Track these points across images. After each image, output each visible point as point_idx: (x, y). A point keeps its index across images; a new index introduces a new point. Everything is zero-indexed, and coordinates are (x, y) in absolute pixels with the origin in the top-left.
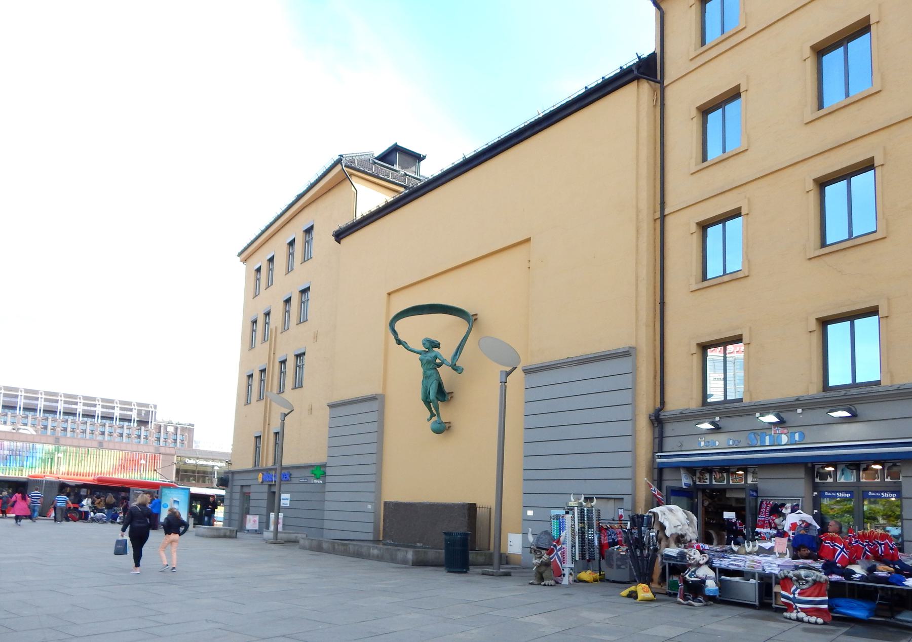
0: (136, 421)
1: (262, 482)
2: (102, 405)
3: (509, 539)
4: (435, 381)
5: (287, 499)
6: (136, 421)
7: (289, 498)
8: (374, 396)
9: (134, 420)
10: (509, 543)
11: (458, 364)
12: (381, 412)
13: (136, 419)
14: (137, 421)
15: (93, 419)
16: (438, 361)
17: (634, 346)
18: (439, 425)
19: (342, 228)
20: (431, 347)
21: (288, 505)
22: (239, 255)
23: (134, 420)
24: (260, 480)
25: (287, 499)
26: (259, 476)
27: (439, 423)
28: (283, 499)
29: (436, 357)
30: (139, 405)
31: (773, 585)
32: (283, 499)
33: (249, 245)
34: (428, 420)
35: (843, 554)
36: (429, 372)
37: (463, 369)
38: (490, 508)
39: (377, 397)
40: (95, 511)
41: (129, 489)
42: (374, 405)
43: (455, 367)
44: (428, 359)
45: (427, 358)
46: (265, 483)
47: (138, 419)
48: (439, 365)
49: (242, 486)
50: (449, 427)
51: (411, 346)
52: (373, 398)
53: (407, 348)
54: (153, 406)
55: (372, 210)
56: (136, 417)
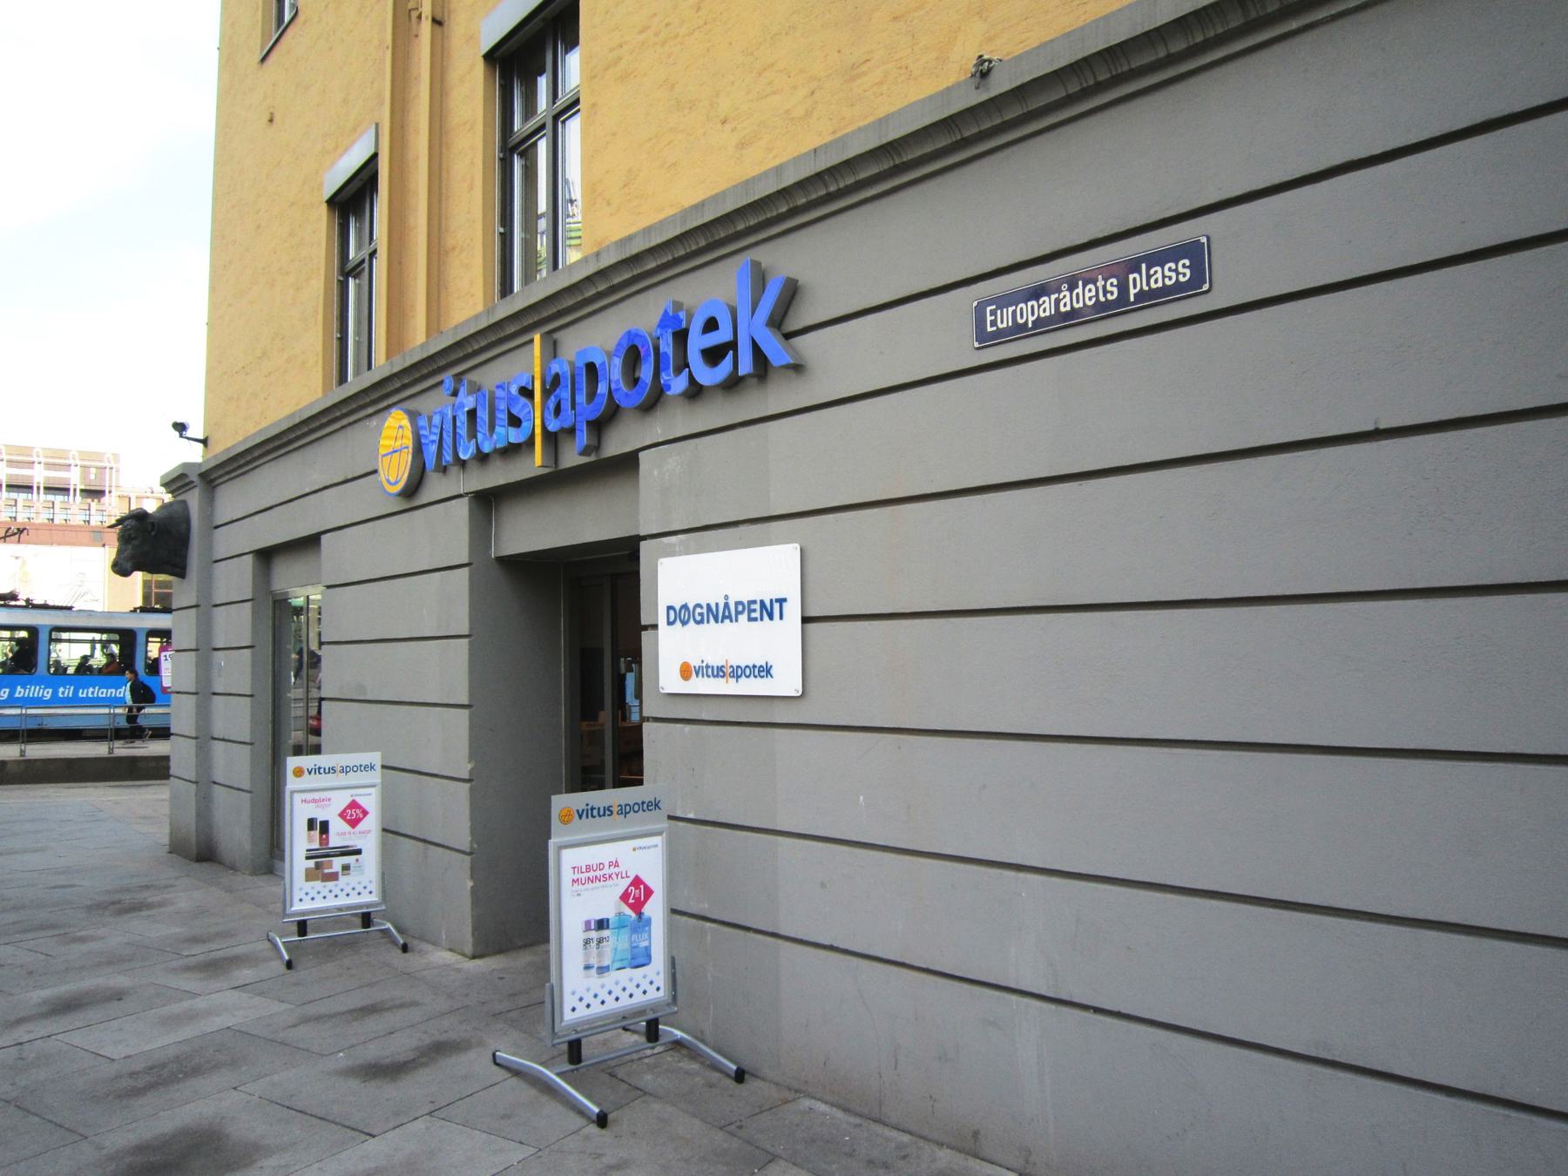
0: (78, 492)
1: (412, 489)
2: (46, 464)
5: (768, 610)
6: (78, 492)
7: (791, 590)
9: (75, 490)
13: (79, 487)
14: (82, 491)
15: (30, 495)
17: (583, 1057)
19: (652, 257)
21: (787, 682)
22: (308, 850)
23: (75, 490)
24: (396, 472)
25: (768, 610)
26: (386, 443)
28: (682, 615)
30: (84, 455)
31: (26, 758)
32: (682, 615)
46: (436, 487)
47: (83, 487)
49: (266, 556)
54: (111, 458)
56: (78, 483)
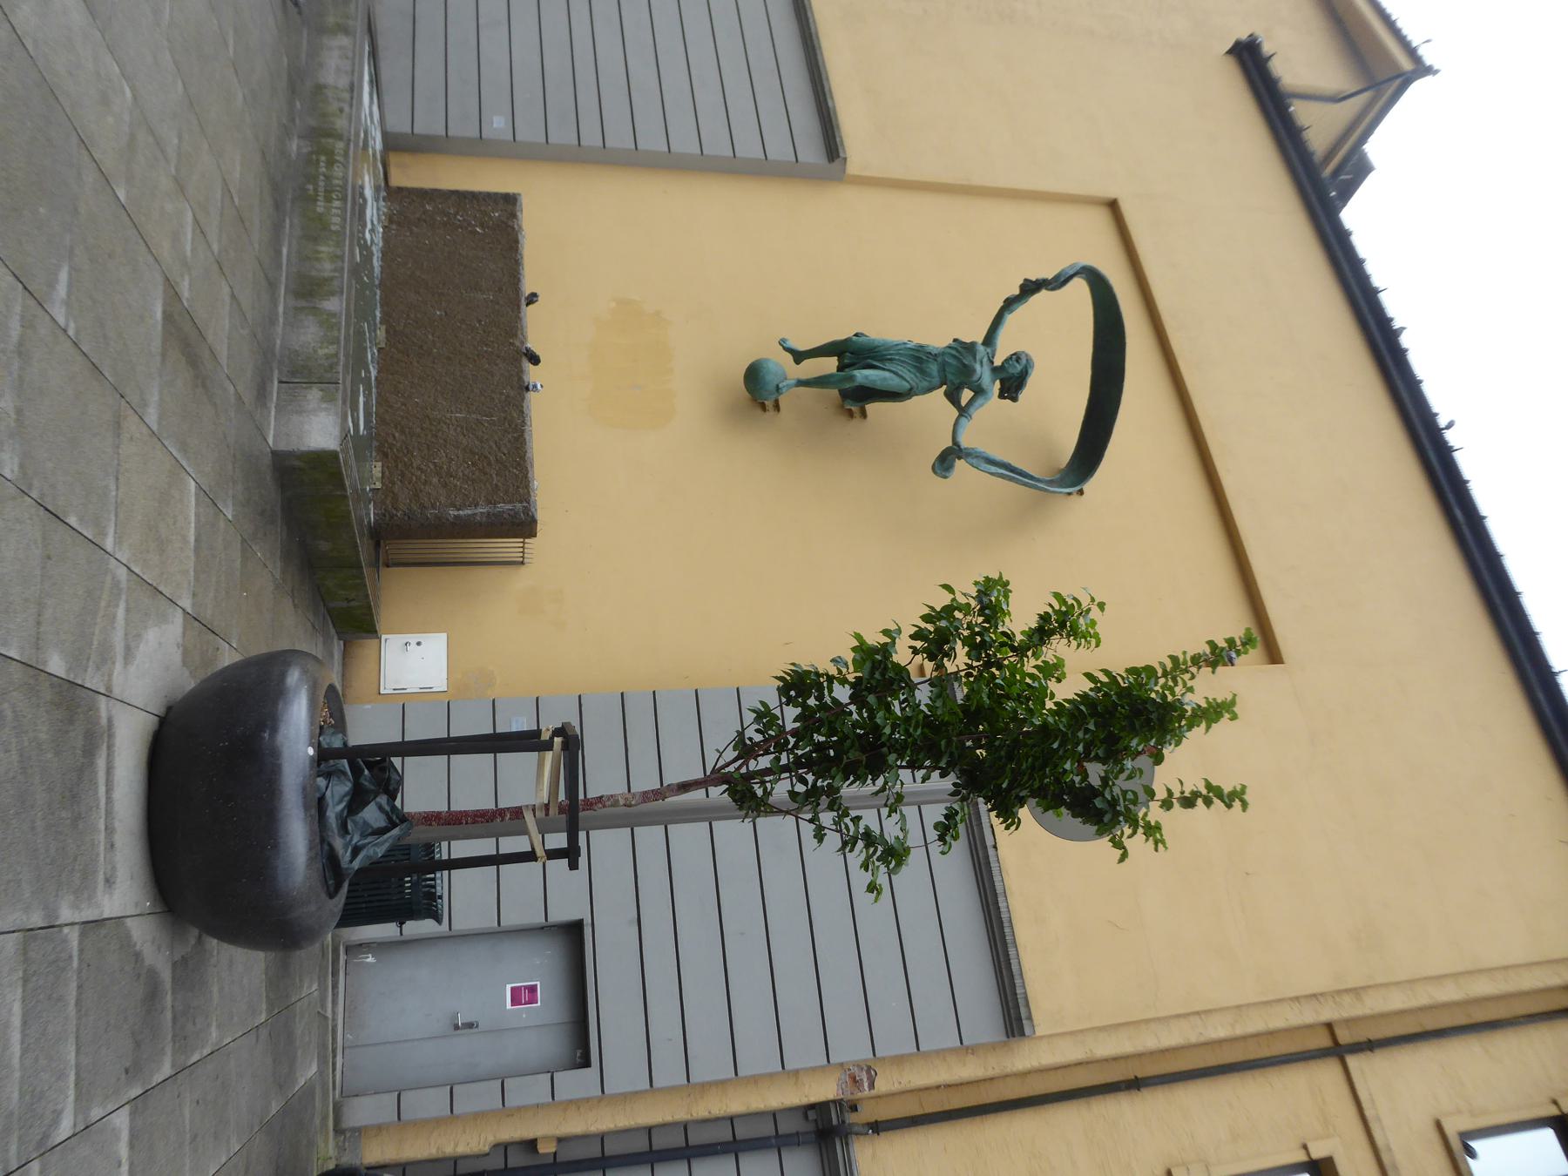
3: (425, 638)
4: (907, 386)
8: (841, 155)
10: (413, 638)
11: (960, 464)
12: (790, 172)
16: (966, 395)
18: (772, 387)
20: (1004, 375)
27: (778, 386)
29: (979, 391)
33: (978, 884)
34: (782, 343)
35: (536, 985)
36: (934, 368)
37: (945, 477)
38: (522, 563)
39: (837, 162)
40: (406, 518)
41: (586, 1063)
42: (811, 152)
43: (945, 461)
44: (974, 371)
45: (978, 367)
48: (953, 397)
50: (763, 407)
51: (1010, 319)
52: (832, 147)
53: (1010, 304)
55: (1371, 279)
